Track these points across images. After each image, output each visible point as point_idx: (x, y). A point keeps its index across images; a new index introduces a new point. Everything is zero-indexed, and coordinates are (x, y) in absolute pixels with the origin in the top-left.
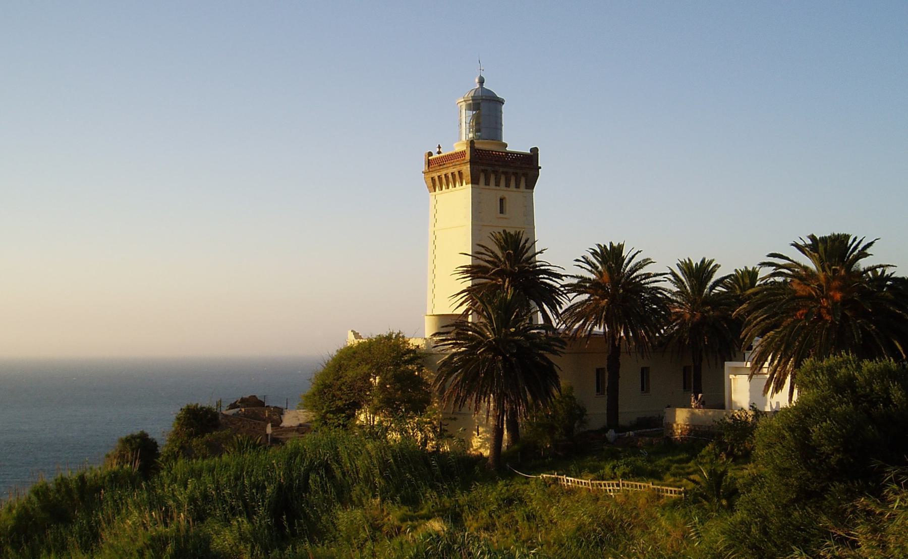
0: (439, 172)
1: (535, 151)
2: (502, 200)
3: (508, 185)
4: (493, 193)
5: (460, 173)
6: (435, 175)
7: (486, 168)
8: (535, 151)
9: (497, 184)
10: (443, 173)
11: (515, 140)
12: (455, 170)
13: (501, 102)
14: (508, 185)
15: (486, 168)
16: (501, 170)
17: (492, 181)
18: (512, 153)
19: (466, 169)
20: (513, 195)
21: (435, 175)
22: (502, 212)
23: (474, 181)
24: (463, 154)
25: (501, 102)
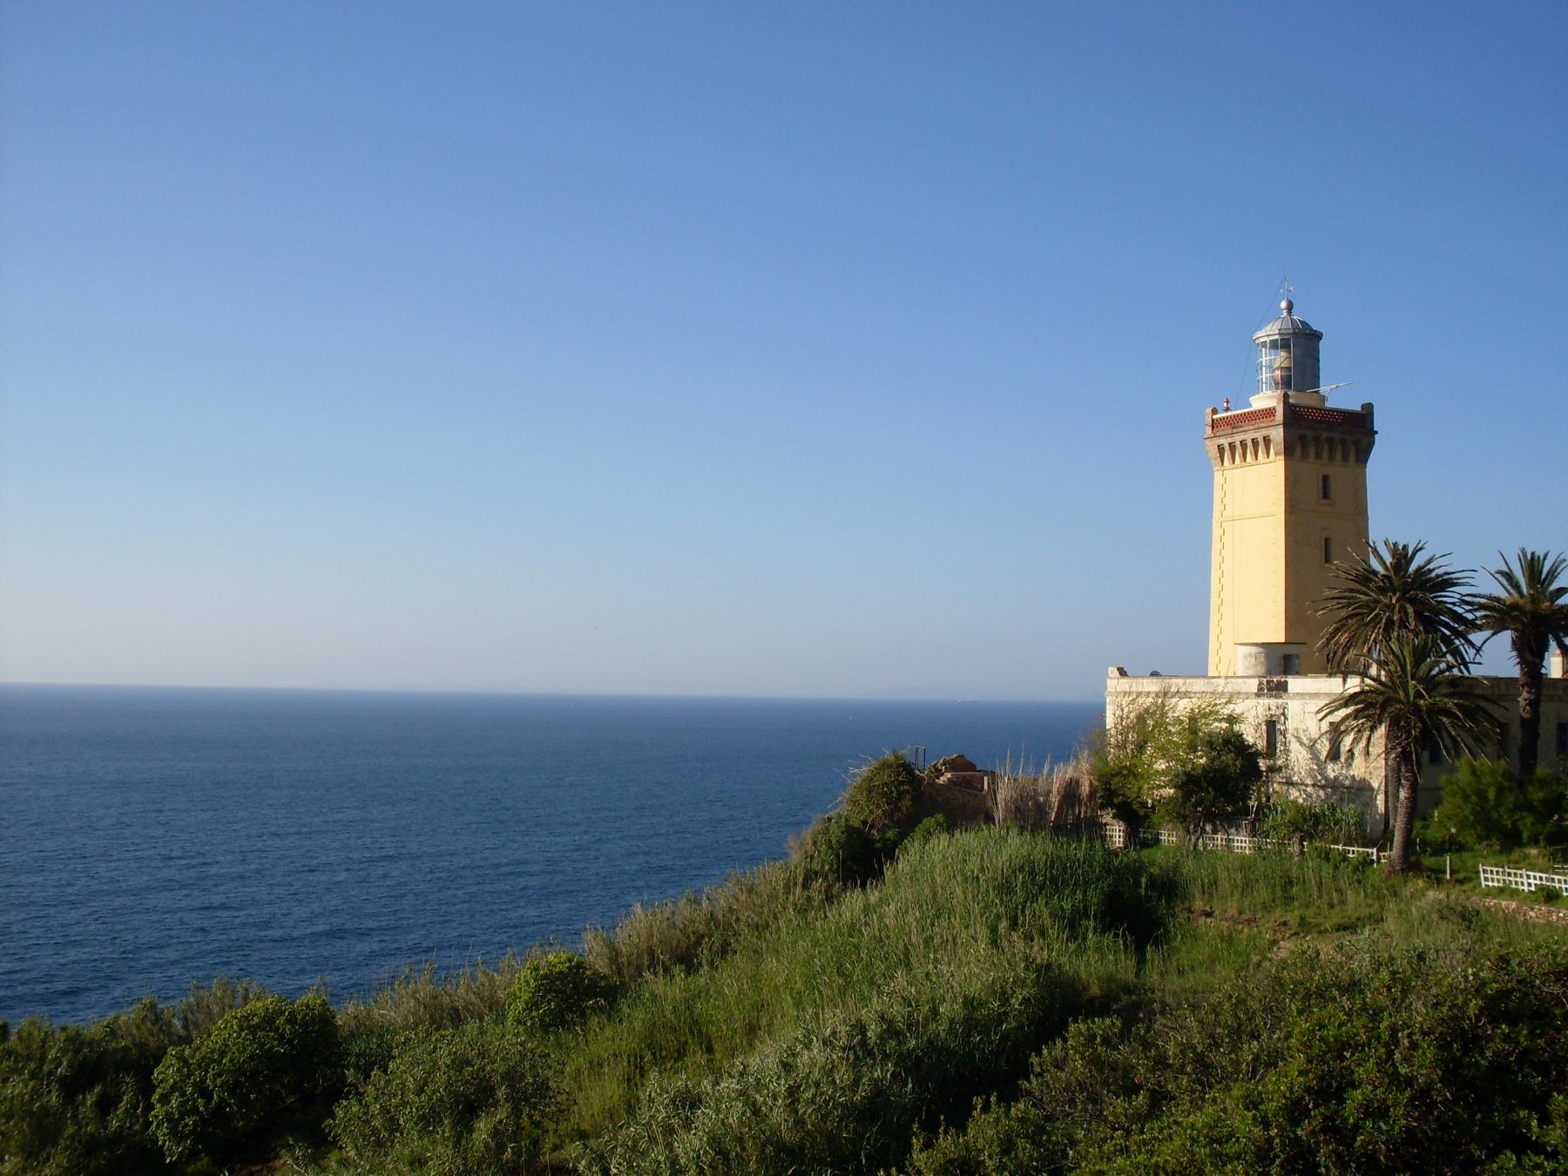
0: (1232, 434)
1: (1368, 409)
2: (1325, 478)
3: (1331, 458)
4: (1311, 469)
5: (1267, 441)
6: (1225, 442)
7: (1398, 838)
8: (1368, 409)
9: (1318, 455)
10: (1237, 439)
11: (1339, 391)
12: (1259, 435)
13: (1317, 336)
14: (1331, 458)
15: (1398, 838)
16: (1325, 435)
17: (1352, 457)
18: (1339, 412)
19: (1277, 434)
20: (1337, 471)
21: (1225, 442)
22: (1326, 495)
23: (1289, 452)
24: (1270, 412)
25: (1317, 336)
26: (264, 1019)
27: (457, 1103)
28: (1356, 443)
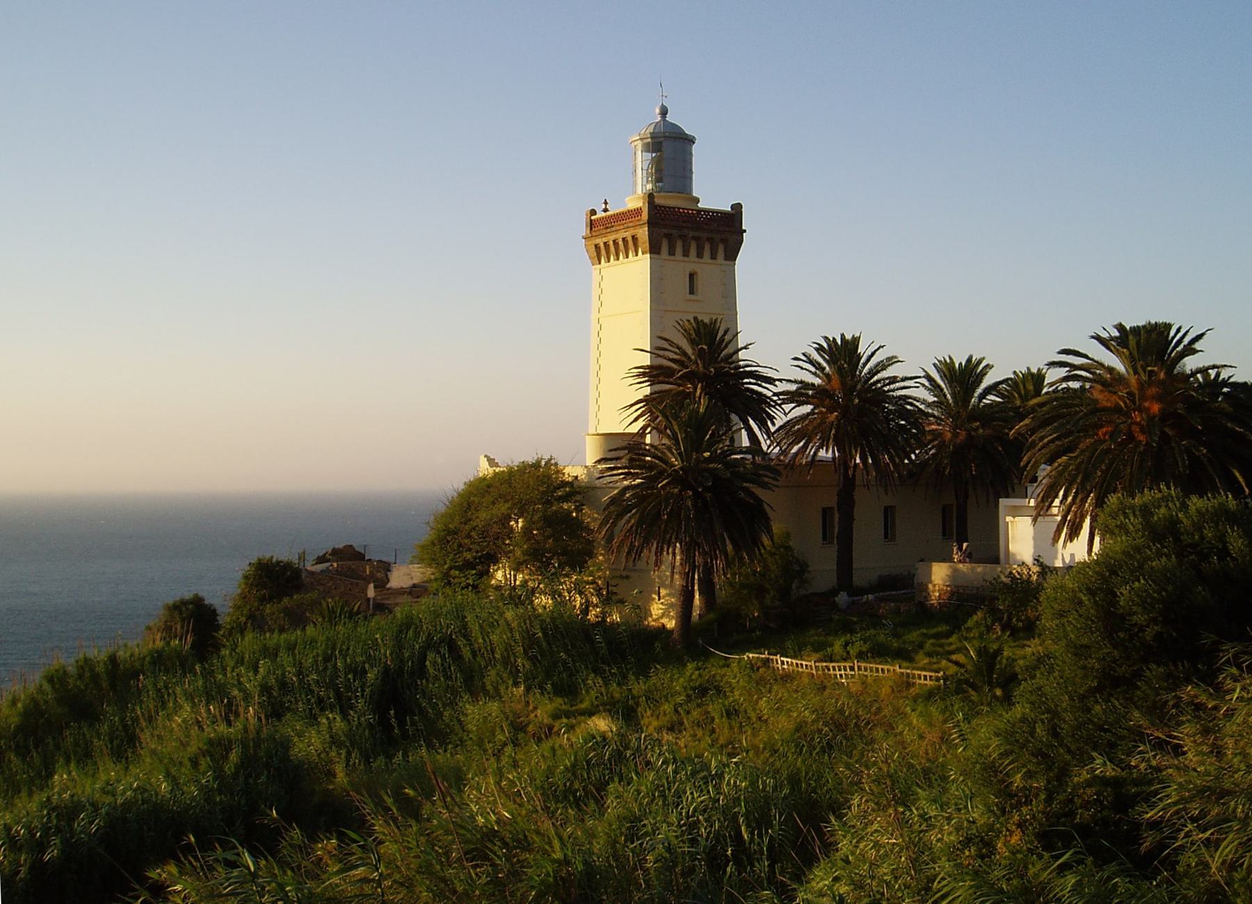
0: (605, 238)
1: (737, 208)
2: (692, 276)
3: (700, 255)
4: (680, 267)
5: (634, 238)
6: (600, 241)
7: (670, 231)
8: (737, 208)
9: (686, 253)
10: (611, 238)
11: (710, 193)
12: (628, 235)
13: (691, 140)
15: (670, 231)
18: (707, 211)
19: (643, 233)
20: (707, 269)
21: (600, 241)
22: (692, 292)
23: (654, 249)
24: (638, 212)
25: (691, 140)
26: (1103, 858)
27: (484, 590)
28: (724, 241)
